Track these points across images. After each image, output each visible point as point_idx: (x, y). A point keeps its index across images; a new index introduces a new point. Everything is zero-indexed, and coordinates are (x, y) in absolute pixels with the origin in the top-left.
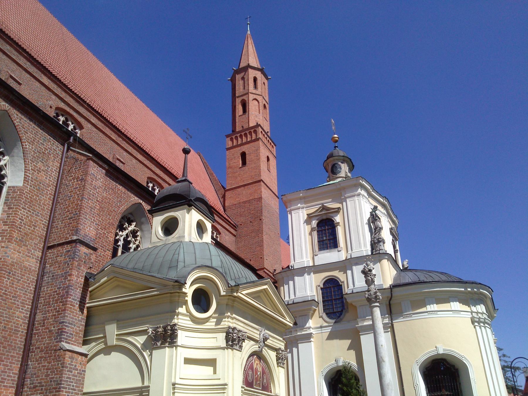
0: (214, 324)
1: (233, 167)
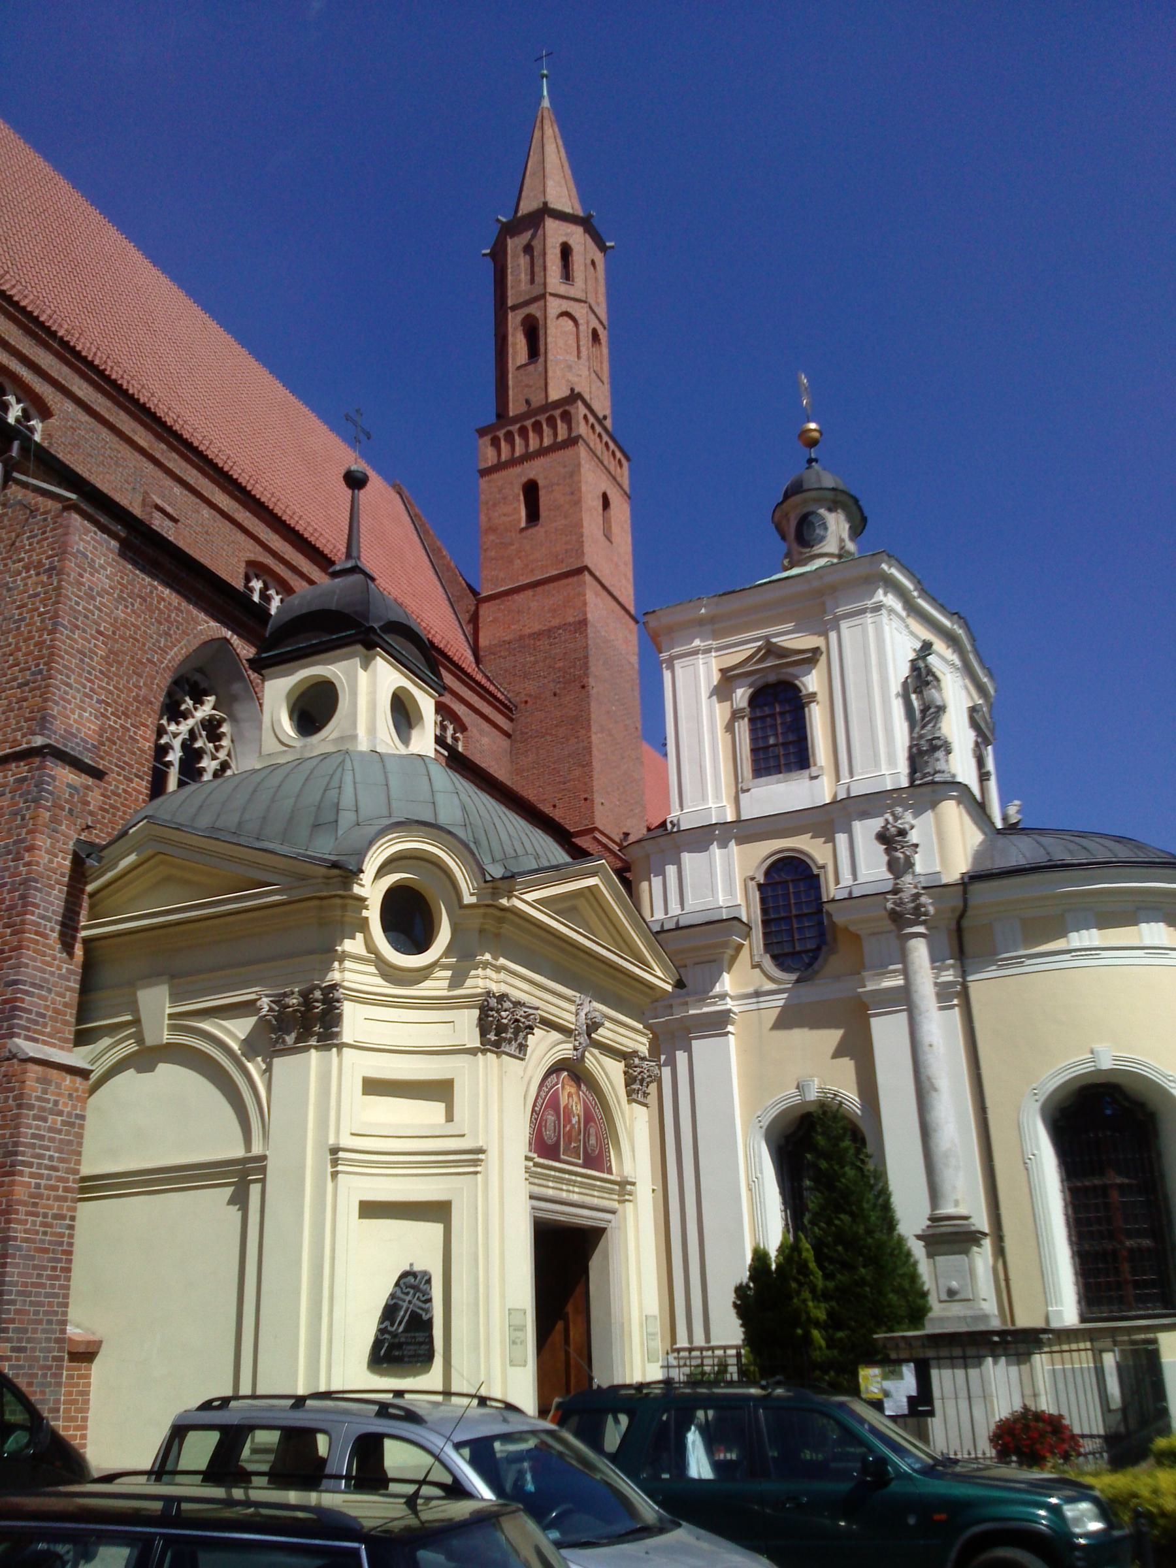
0: (446, 983)
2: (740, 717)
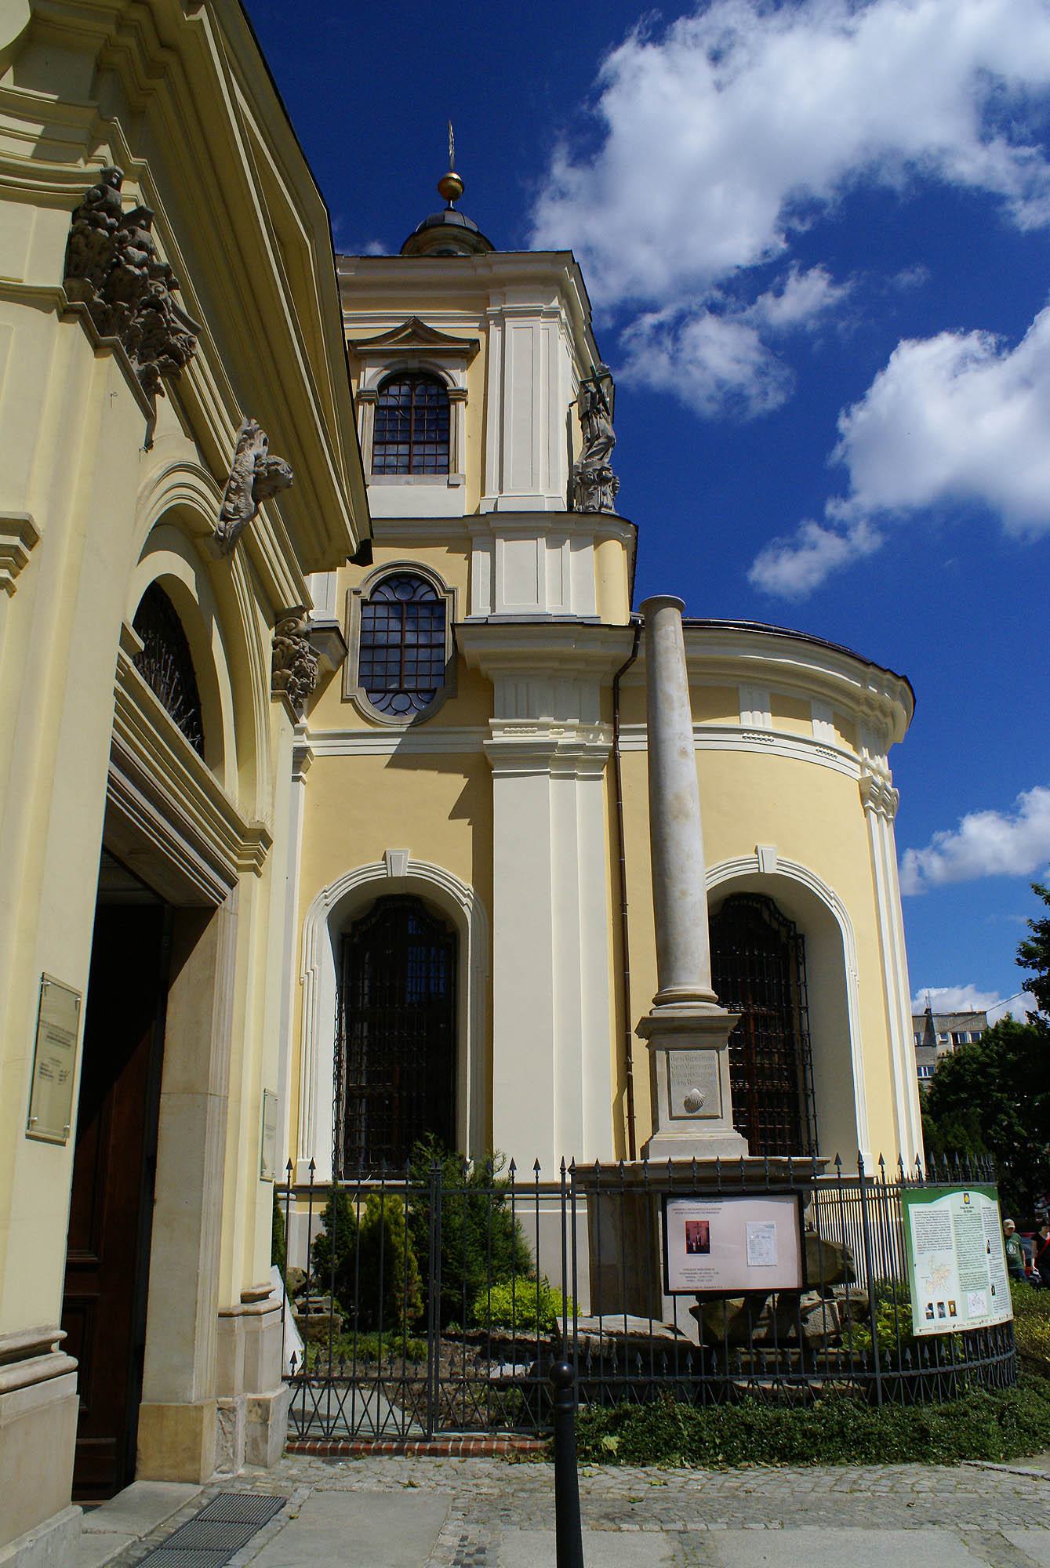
2: (366, 401)
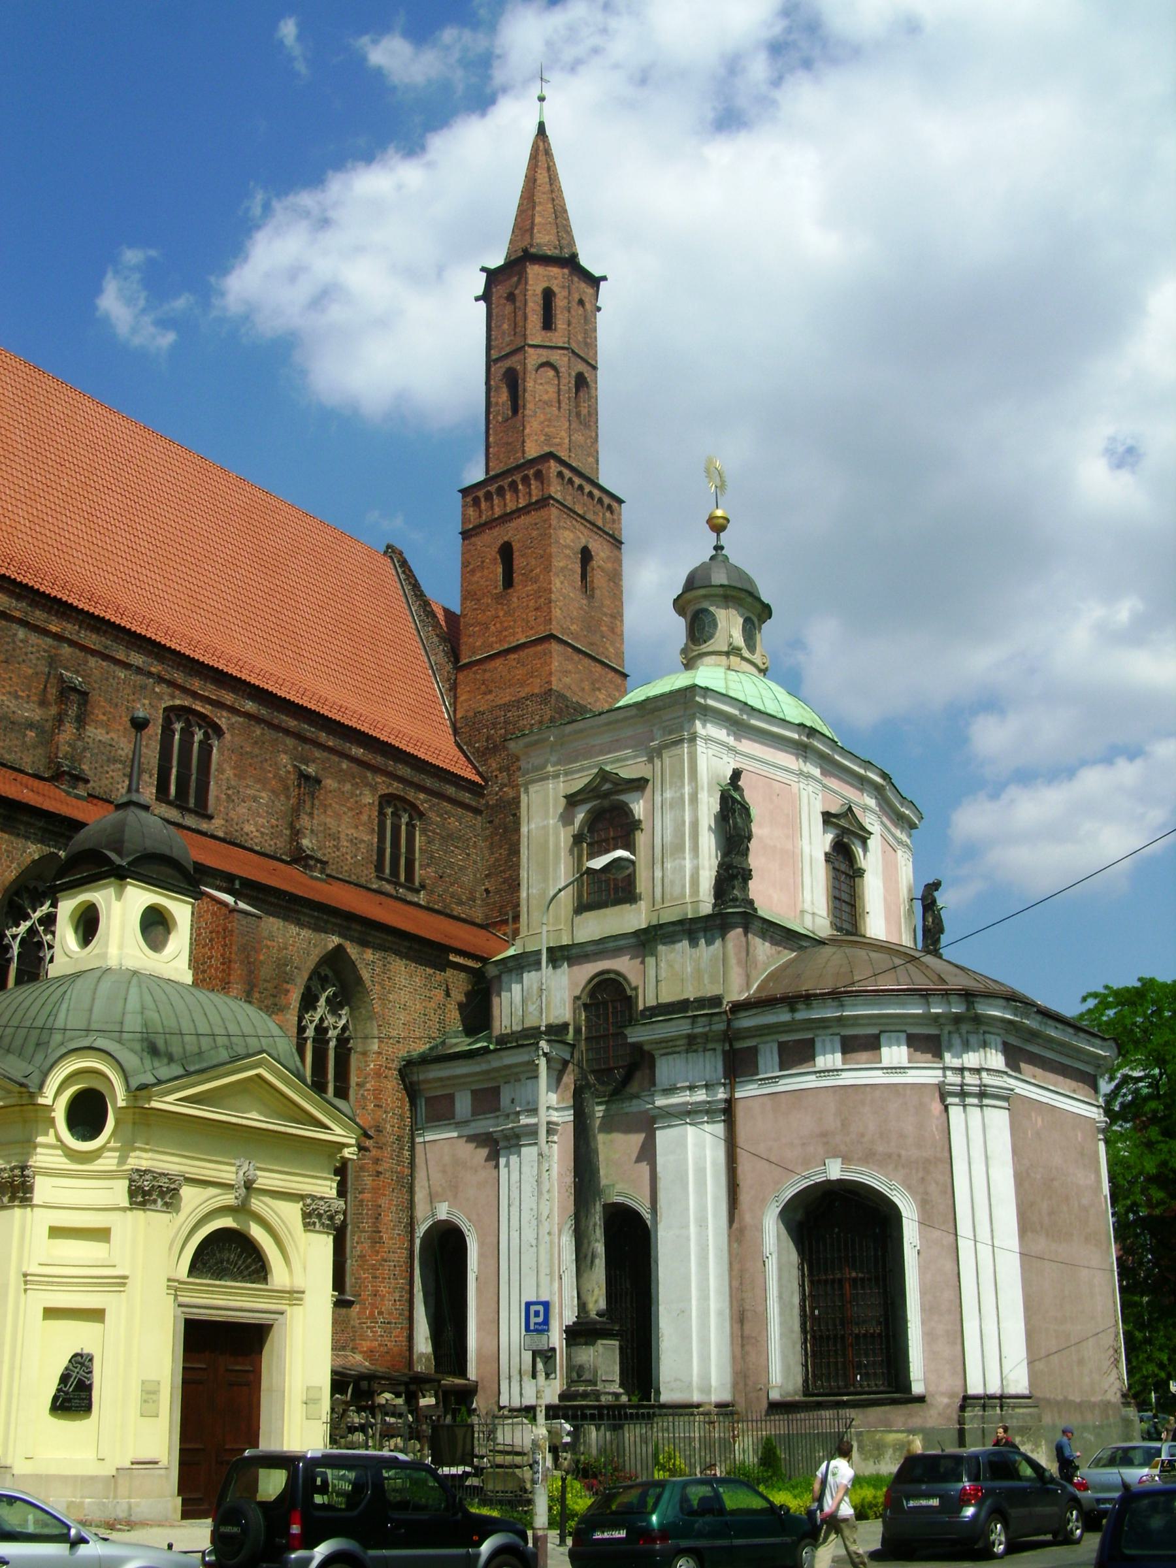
0: (116, 1161)
1: (478, 593)
